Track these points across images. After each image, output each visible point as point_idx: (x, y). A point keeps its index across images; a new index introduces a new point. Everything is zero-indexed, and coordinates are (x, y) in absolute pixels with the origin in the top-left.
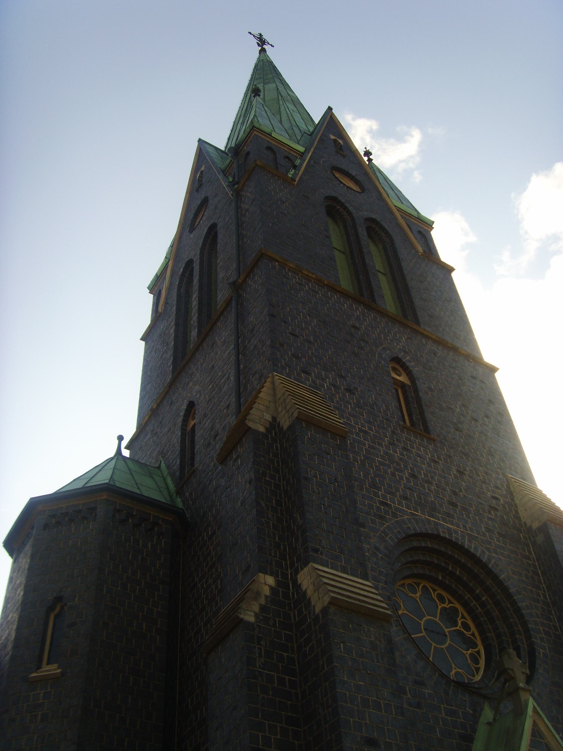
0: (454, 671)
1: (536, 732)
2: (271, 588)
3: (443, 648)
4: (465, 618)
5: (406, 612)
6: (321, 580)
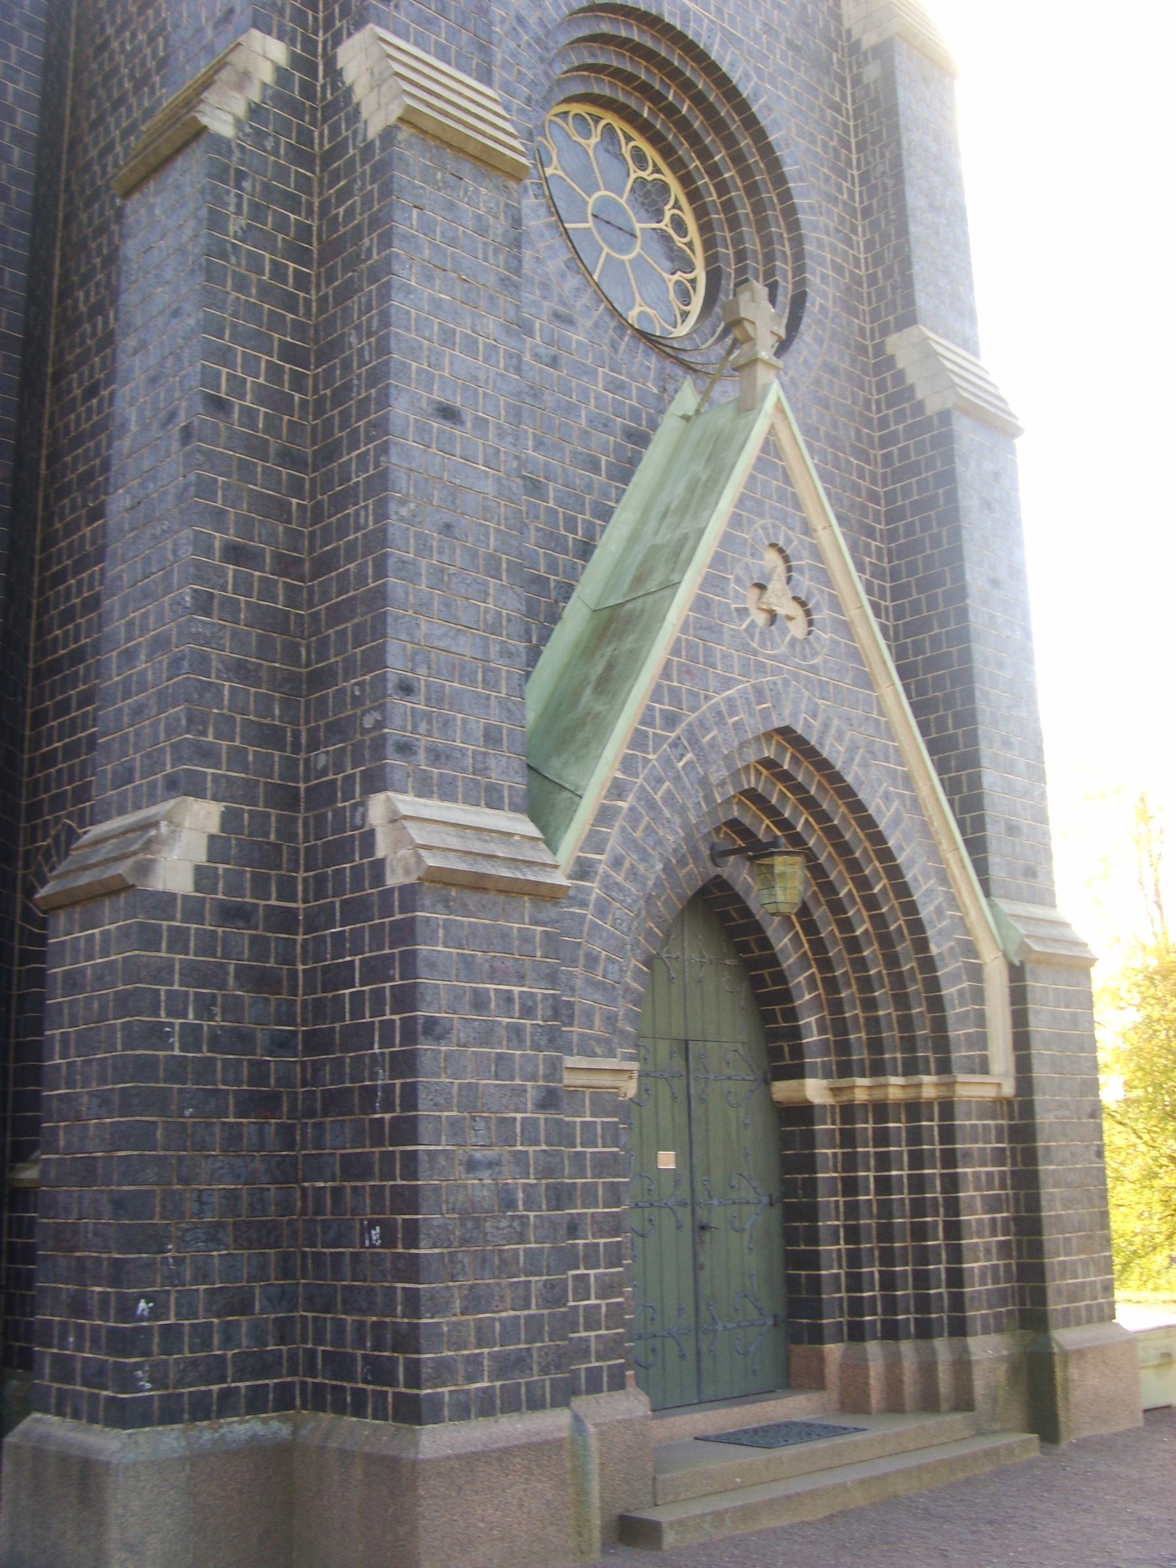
0: (637, 310)
1: (770, 446)
2: (278, 69)
3: (623, 262)
4: (680, 208)
5: (561, 173)
6: (390, 67)
